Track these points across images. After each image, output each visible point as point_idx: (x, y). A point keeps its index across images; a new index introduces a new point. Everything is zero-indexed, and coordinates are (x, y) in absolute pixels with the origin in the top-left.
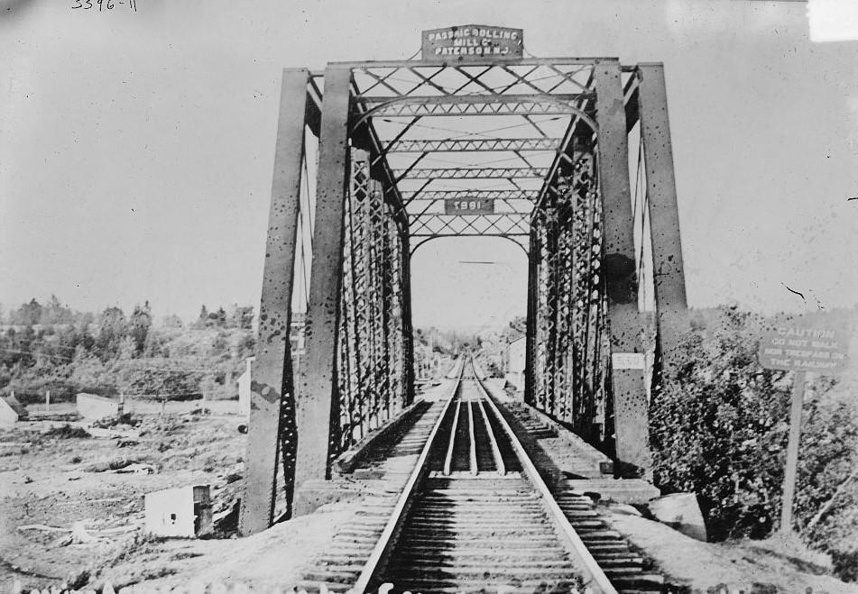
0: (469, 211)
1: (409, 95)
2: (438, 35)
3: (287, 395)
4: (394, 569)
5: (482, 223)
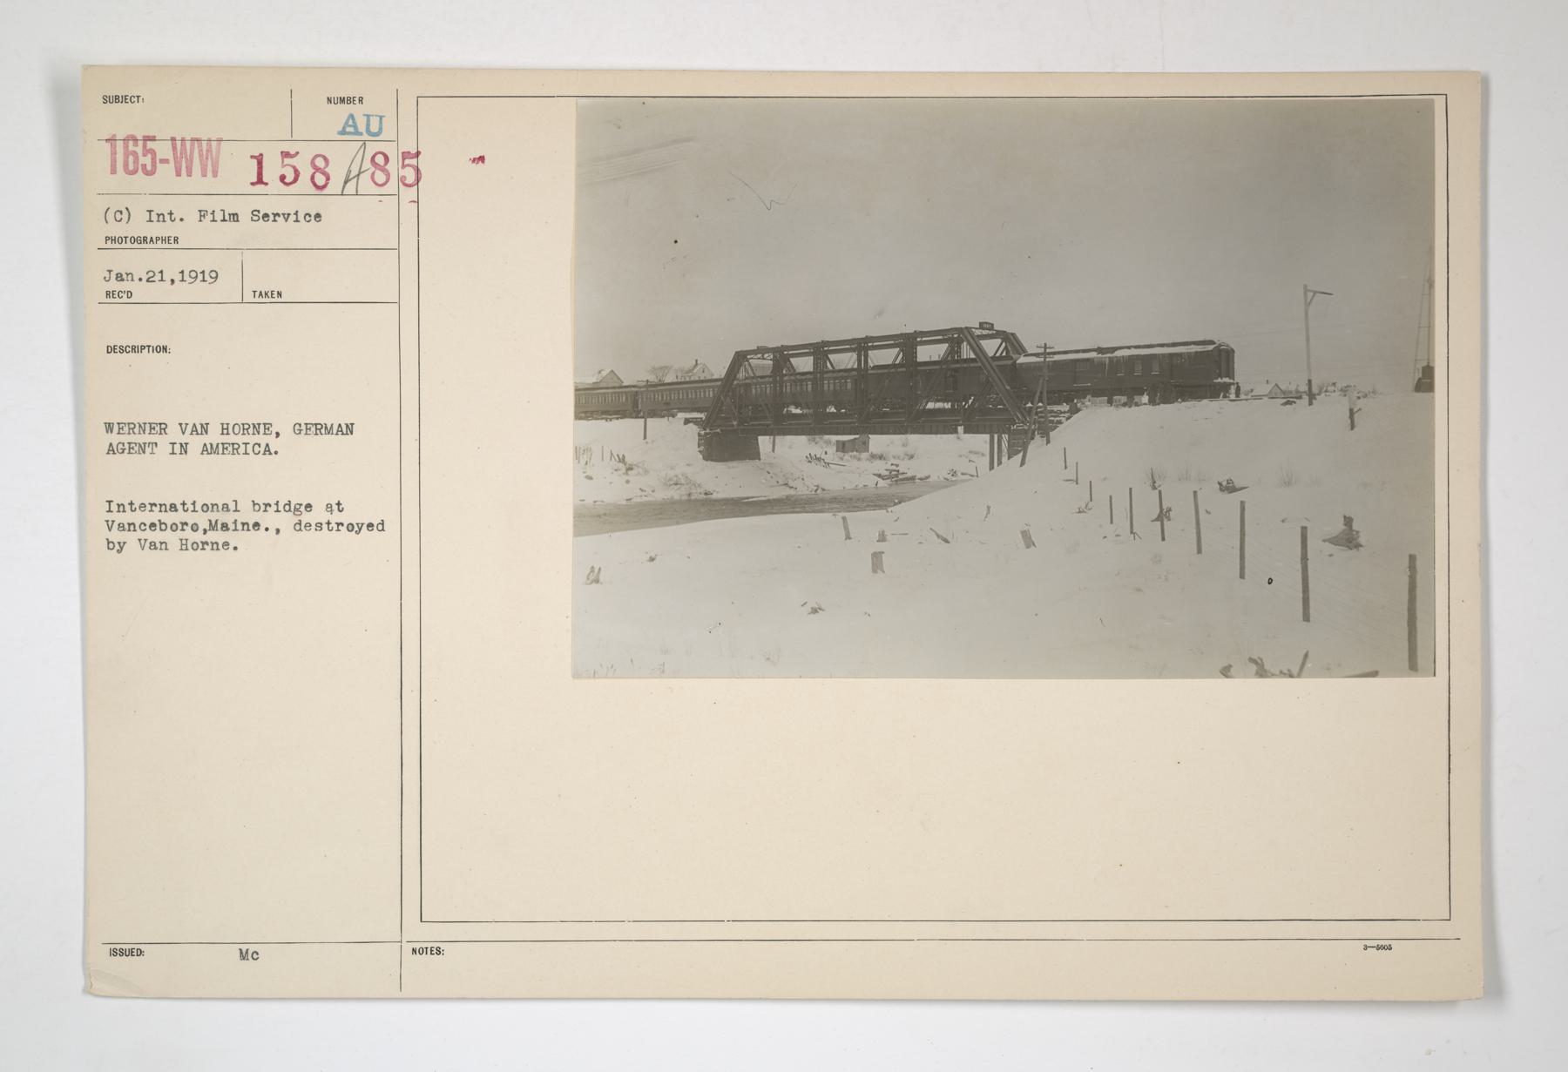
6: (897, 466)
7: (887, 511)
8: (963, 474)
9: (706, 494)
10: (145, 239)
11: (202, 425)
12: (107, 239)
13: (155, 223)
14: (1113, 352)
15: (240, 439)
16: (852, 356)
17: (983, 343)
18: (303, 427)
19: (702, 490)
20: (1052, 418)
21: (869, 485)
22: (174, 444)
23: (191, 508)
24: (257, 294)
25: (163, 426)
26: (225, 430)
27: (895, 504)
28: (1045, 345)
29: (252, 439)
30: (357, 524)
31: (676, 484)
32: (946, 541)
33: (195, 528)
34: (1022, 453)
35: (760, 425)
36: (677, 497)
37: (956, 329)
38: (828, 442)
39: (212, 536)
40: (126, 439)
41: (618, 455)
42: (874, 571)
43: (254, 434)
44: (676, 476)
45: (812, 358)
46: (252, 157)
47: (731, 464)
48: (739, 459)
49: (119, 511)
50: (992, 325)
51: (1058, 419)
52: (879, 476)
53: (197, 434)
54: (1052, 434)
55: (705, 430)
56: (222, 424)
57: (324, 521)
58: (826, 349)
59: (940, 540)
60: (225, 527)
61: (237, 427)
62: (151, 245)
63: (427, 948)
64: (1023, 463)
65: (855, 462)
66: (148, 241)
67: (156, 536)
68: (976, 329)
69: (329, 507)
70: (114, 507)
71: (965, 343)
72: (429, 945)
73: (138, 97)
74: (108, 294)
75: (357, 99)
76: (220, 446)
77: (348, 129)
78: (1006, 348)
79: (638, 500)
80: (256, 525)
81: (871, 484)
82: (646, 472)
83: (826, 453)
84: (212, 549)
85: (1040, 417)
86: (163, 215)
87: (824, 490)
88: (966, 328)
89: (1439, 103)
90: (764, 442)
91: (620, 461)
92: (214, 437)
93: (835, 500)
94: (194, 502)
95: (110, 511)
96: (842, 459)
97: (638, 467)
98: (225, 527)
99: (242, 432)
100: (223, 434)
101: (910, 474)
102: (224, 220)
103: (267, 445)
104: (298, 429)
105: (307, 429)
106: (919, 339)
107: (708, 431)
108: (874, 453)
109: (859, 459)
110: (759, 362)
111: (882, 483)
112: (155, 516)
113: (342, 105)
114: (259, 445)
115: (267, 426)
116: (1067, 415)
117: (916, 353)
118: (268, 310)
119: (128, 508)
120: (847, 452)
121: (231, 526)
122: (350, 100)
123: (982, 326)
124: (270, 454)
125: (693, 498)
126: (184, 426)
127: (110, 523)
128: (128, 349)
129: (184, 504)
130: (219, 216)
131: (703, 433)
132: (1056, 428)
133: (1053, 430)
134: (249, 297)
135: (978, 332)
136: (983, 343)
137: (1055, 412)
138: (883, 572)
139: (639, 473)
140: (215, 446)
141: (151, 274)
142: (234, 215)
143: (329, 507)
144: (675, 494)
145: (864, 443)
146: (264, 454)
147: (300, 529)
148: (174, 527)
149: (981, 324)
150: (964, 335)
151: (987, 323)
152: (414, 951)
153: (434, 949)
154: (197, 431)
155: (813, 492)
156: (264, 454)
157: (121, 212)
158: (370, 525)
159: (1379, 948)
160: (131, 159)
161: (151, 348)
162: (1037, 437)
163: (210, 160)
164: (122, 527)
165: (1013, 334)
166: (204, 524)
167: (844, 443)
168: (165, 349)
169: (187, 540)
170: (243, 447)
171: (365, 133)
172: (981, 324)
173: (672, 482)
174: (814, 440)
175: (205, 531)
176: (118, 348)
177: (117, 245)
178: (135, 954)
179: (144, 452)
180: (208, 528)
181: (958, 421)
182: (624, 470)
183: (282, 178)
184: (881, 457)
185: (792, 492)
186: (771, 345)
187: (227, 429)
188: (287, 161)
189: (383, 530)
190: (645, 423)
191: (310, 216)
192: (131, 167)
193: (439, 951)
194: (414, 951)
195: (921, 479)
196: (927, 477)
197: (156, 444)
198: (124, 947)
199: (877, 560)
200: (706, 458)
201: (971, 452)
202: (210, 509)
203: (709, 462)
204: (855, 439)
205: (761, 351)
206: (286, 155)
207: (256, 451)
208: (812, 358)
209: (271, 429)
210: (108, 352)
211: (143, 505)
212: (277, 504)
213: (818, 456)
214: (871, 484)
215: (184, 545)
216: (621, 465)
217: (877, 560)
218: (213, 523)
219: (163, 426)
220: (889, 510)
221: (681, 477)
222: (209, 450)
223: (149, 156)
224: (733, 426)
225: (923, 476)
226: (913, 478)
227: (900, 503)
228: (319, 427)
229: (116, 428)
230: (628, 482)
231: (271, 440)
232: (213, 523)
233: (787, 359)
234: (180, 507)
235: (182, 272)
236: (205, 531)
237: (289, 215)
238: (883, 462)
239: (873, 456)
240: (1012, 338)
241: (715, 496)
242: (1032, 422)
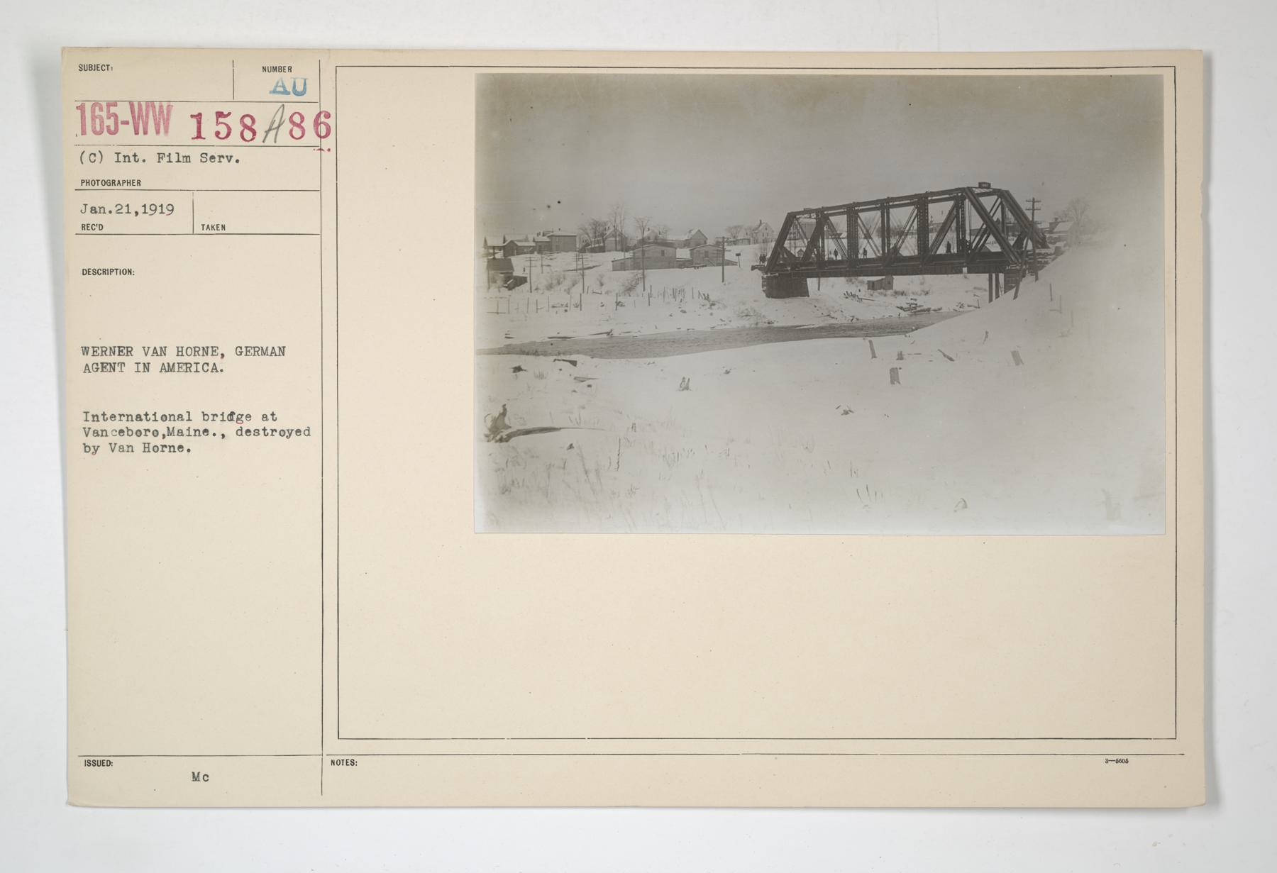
6: (915, 300)
7: (906, 336)
8: (969, 306)
9: (769, 323)
10: (114, 182)
11: (161, 348)
12: (83, 182)
13: (122, 163)
15: (192, 360)
16: (877, 214)
17: (982, 199)
18: (244, 350)
19: (766, 320)
20: (1040, 260)
21: (894, 316)
22: (138, 363)
23: (153, 418)
24: (205, 227)
25: (130, 349)
26: (180, 351)
27: (913, 330)
28: (1034, 199)
29: (201, 360)
30: (288, 430)
31: (747, 316)
32: (951, 359)
33: (156, 433)
34: (1014, 289)
35: (808, 270)
36: (747, 326)
37: (960, 189)
38: (862, 282)
39: (169, 441)
40: (100, 359)
41: (704, 295)
42: (892, 382)
43: (203, 355)
44: (747, 309)
45: (846, 216)
46: (192, 116)
47: (787, 300)
48: (793, 296)
49: (94, 421)
50: (989, 184)
51: (1046, 260)
52: (901, 308)
53: (158, 355)
54: (1040, 273)
55: (767, 274)
56: (178, 347)
57: (261, 428)
58: (856, 208)
59: (946, 359)
60: (180, 433)
61: (189, 350)
62: (119, 187)
63: (343, 760)
64: (1015, 297)
65: (882, 298)
66: (116, 183)
67: (124, 441)
68: (976, 188)
69: (265, 417)
70: (90, 418)
71: (967, 200)
73: (108, 66)
75: (287, 68)
76: (176, 366)
77: (278, 89)
78: (1001, 203)
79: (719, 328)
80: (206, 431)
81: (895, 315)
82: (725, 306)
83: (860, 291)
84: (170, 451)
85: (1030, 259)
87: (857, 319)
88: (968, 188)
89: (1168, 75)
90: (812, 283)
91: (705, 299)
92: (171, 357)
93: (862, 329)
94: (155, 413)
95: (86, 420)
96: (872, 295)
97: (719, 303)
98: (180, 433)
99: (193, 354)
100: (178, 355)
101: (925, 307)
102: (178, 161)
103: (214, 364)
104: (239, 351)
105: (247, 351)
106: (929, 198)
107: (769, 275)
108: (898, 290)
109: (885, 295)
110: (807, 220)
111: (903, 314)
112: (123, 424)
113: (275, 73)
114: (208, 364)
115: (214, 349)
116: (1052, 257)
117: (927, 209)
119: (101, 418)
120: (876, 290)
121: (185, 432)
122: (281, 69)
123: (981, 185)
124: (217, 371)
125: (759, 325)
126: (146, 349)
127: (87, 430)
128: (100, 272)
129: (146, 415)
130: (174, 158)
131: (765, 276)
132: (1043, 267)
133: (1041, 269)
134: (198, 229)
135: (978, 191)
136: (982, 199)
137: (1043, 255)
138: (899, 383)
139: (718, 308)
140: (171, 365)
141: (119, 207)
142: (186, 157)
143: (265, 417)
144: (746, 323)
145: (889, 283)
146: (212, 372)
147: (241, 435)
148: (139, 433)
149: (980, 184)
150: (966, 193)
151: (985, 183)
152: (333, 762)
154: (157, 353)
155: (850, 322)
156: (212, 372)
157: (95, 155)
158: (298, 431)
159: (1117, 761)
160: (98, 121)
161: (118, 271)
162: (1028, 275)
163: (141, 122)
164: (96, 433)
165: (1007, 192)
166: (163, 431)
167: (873, 283)
169: (149, 444)
170: (194, 366)
171: (292, 93)
172: (980, 184)
173: (743, 314)
174: (851, 281)
175: (164, 436)
176: (91, 270)
177: (91, 187)
178: (105, 764)
179: (114, 370)
180: (166, 434)
181: (963, 263)
182: (708, 306)
183: (217, 134)
184: (903, 294)
185: (833, 321)
186: (814, 207)
187: (182, 351)
188: (221, 120)
189: (309, 435)
193: (353, 763)
194: (333, 762)
195: (935, 310)
196: (940, 309)
197: (124, 363)
198: (96, 759)
199: (894, 376)
200: (768, 296)
201: (975, 288)
202: (168, 419)
203: (771, 299)
204: (882, 279)
205: (808, 211)
206: (220, 114)
207: (205, 369)
208: (846, 216)
209: (217, 351)
210: (83, 274)
211: (113, 417)
212: (223, 414)
213: (853, 293)
214: (895, 315)
215: (146, 448)
216: (706, 302)
217: (894, 376)
218: (171, 430)
219: (130, 349)
220: (907, 335)
221: (749, 310)
222: (167, 368)
223: (112, 118)
224: (787, 270)
225: (936, 308)
226: (929, 310)
227: (916, 329)
228: (257, 349)
229: (91, 351)
230: (711, 314)
231: (217, 360)
232: (171, 430)
233: (826, 217)
234: (143, 417)
235: (145, 206)
236: (164, 436)
238: (904, 297)
239: (896, 293)
240: (1006, 195)
241: (776, 325)
242: (1024, 262)
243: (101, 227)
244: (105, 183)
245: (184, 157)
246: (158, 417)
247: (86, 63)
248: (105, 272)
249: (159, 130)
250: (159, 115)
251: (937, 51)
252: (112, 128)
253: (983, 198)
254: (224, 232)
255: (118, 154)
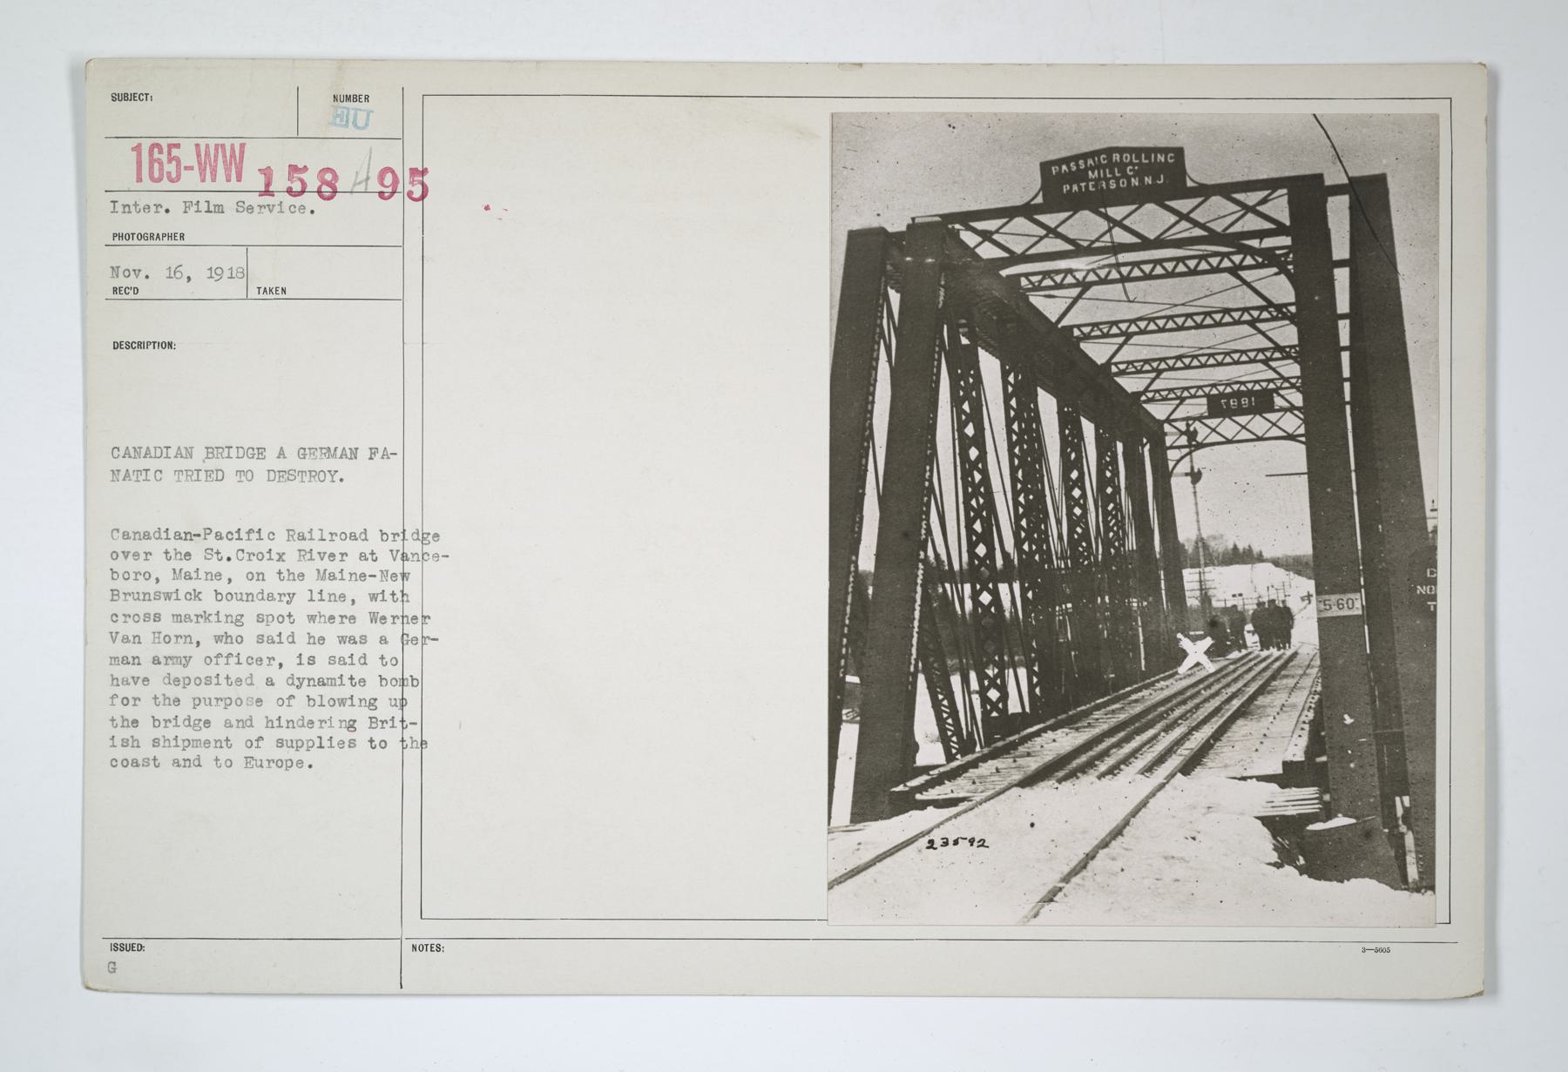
0: (1242, 411)
1: (1030, 252)
2: (1064, 167)
3: (856, 535)
4: (1071, 698)
5: (1258, 424)
10: (152, 236)
12: (115, 235)
14: (1009, 554)
24: (262, 290)
62: (158, 242)
63: (427, 945)
66: (155, 237)
72: (429, 942)
73: (147, 94)
74: (115, 290)
86: (129, 206)
102: (208, 211)
118: (273, 306)
128: (134, 345)
130: (203, 206)
134: (253, 293)
153: (435, 946)
156: (124, 457)
159: (1377, 951)
160: (156, 166)
161: (156, 345)
168: (170, 345)
176: (123, 343)
177: (125, 242)
178: (136, 949)
190: (1217, 426)
191: (295, 207)
192: (156, 174)
193: (439, 948)
194: (414, 947)
198: (124, 942)
210: (114, 348)
223: (174, 163)
235: (211, 269)
237: (273, 206)
243: (136, 290)
244: (142, 236)
245: (215, 206)
246: (171, 535)
247: (121, 91)
248: (140, 345)
249: (230, 176)
250: (231, 156)
251: (1161, 63)
252: (174, 175)
253: (1340, 182)
254: (284, 296)
255: (114, 202)
